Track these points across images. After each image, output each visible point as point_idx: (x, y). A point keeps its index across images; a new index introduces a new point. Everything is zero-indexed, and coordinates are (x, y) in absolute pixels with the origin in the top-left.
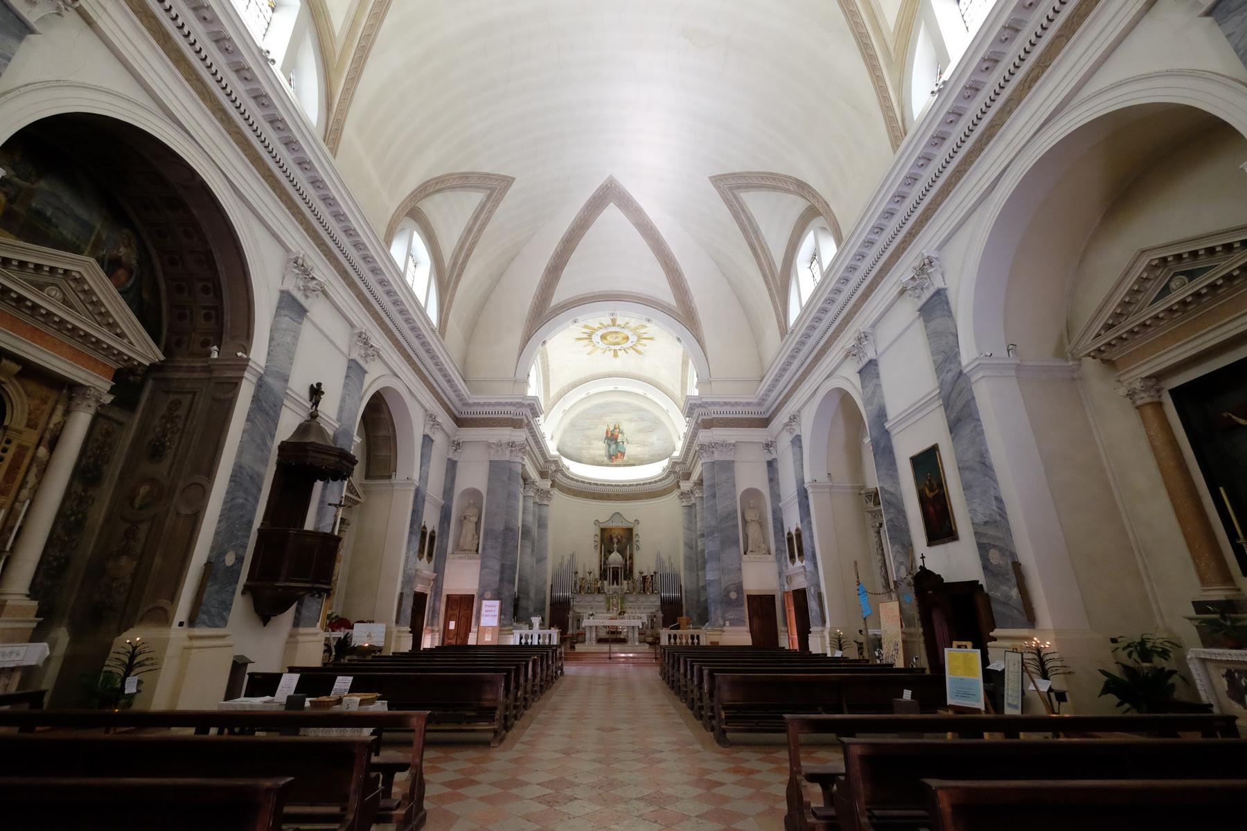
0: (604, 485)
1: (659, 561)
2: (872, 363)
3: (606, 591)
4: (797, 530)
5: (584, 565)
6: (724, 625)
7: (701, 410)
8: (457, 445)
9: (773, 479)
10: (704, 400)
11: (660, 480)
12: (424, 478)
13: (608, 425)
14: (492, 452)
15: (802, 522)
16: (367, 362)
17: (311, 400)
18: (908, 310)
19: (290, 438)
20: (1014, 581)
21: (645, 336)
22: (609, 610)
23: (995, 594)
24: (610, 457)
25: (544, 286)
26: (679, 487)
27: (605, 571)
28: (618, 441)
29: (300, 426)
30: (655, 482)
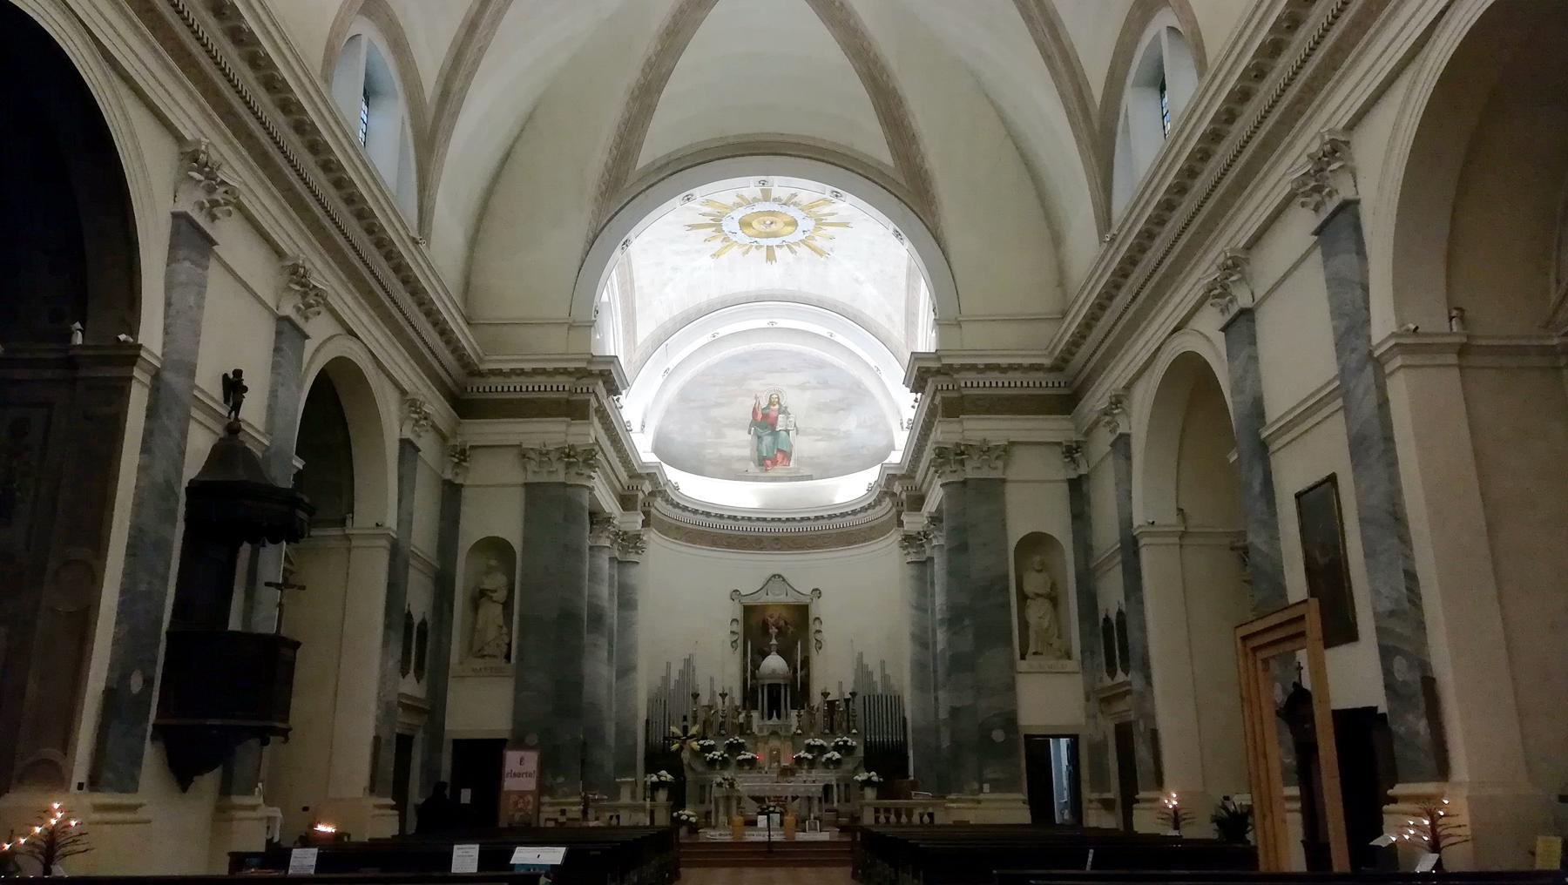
0: (750, 519)
1: (862, 671)
2: (1247, 314)
3: (755, 729)
4: (1120, 613)
5: (712, 680)
6: (981, 790)
7: (943, 381)
8: (461, 455)
9: (1080, 514)
10: (946, 361)
11: (864, 509)
12: (405, 520)
13: (756, 398)
14: (532, 466)
15: (1127, 598)
16: (307, 318)
17: (226, 401)
18: (1300, 227)
19: (197, 477)
20: (1423, 706)
21: (830, 219)
23: (1399, 728)
24: (762, 462)
25: (623, 127)
26: (900, 524)
27: (754, 690)
29: (214, 449)
30: (854, 512)
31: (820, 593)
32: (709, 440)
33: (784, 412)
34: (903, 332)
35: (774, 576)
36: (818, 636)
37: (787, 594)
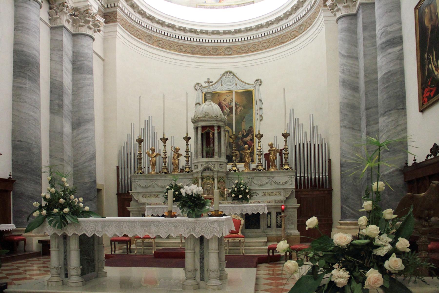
31: (261, 82)
37: (236, 85)
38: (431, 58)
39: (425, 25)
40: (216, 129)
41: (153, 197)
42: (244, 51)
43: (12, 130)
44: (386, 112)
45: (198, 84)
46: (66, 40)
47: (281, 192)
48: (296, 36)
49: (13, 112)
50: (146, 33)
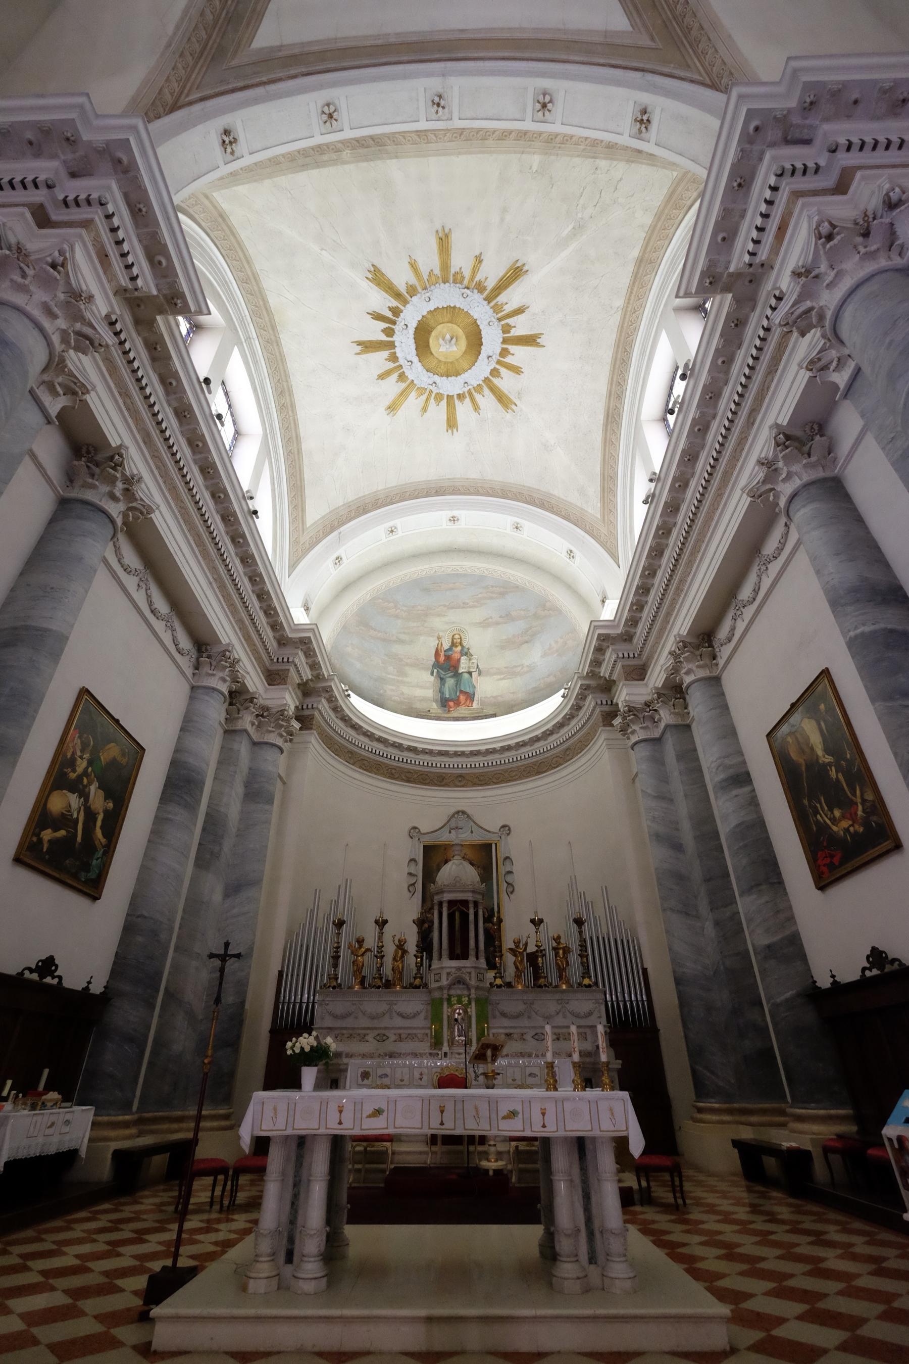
11: (560, 725)
22: (437, 1043)
24: (444, 703)
28: (461, 671)
31: (509, 829)
32: (391, 676)
33: (466, 654)
34: (599, 505)
35: (458, 812)
36: (509, 878)
37: (472, 832)
38: (818, 805)
39: (793, 760)
40: (471, 906)
41: (355, 1040)
42: (483, 783)
43: (134, 894)
44: (752, 888)
45: (415, 828)
46: (243, 749)
47: (585, 1033)
48: (561, 764)
49: (143, 861)
50: (346, 747)
